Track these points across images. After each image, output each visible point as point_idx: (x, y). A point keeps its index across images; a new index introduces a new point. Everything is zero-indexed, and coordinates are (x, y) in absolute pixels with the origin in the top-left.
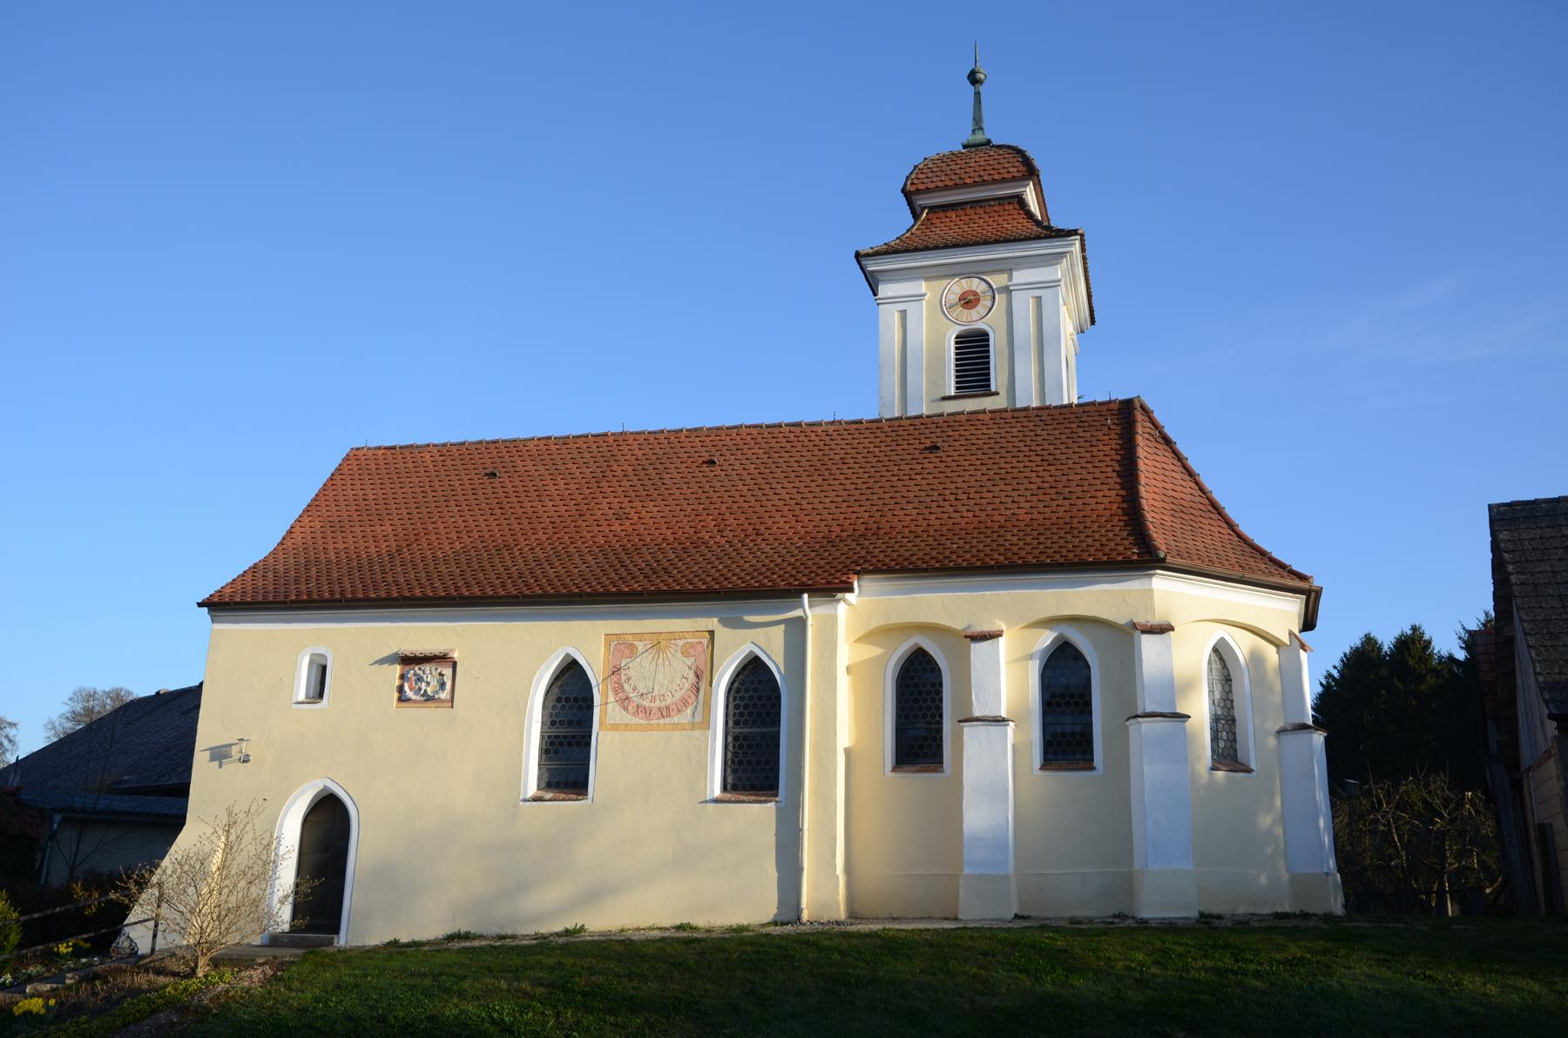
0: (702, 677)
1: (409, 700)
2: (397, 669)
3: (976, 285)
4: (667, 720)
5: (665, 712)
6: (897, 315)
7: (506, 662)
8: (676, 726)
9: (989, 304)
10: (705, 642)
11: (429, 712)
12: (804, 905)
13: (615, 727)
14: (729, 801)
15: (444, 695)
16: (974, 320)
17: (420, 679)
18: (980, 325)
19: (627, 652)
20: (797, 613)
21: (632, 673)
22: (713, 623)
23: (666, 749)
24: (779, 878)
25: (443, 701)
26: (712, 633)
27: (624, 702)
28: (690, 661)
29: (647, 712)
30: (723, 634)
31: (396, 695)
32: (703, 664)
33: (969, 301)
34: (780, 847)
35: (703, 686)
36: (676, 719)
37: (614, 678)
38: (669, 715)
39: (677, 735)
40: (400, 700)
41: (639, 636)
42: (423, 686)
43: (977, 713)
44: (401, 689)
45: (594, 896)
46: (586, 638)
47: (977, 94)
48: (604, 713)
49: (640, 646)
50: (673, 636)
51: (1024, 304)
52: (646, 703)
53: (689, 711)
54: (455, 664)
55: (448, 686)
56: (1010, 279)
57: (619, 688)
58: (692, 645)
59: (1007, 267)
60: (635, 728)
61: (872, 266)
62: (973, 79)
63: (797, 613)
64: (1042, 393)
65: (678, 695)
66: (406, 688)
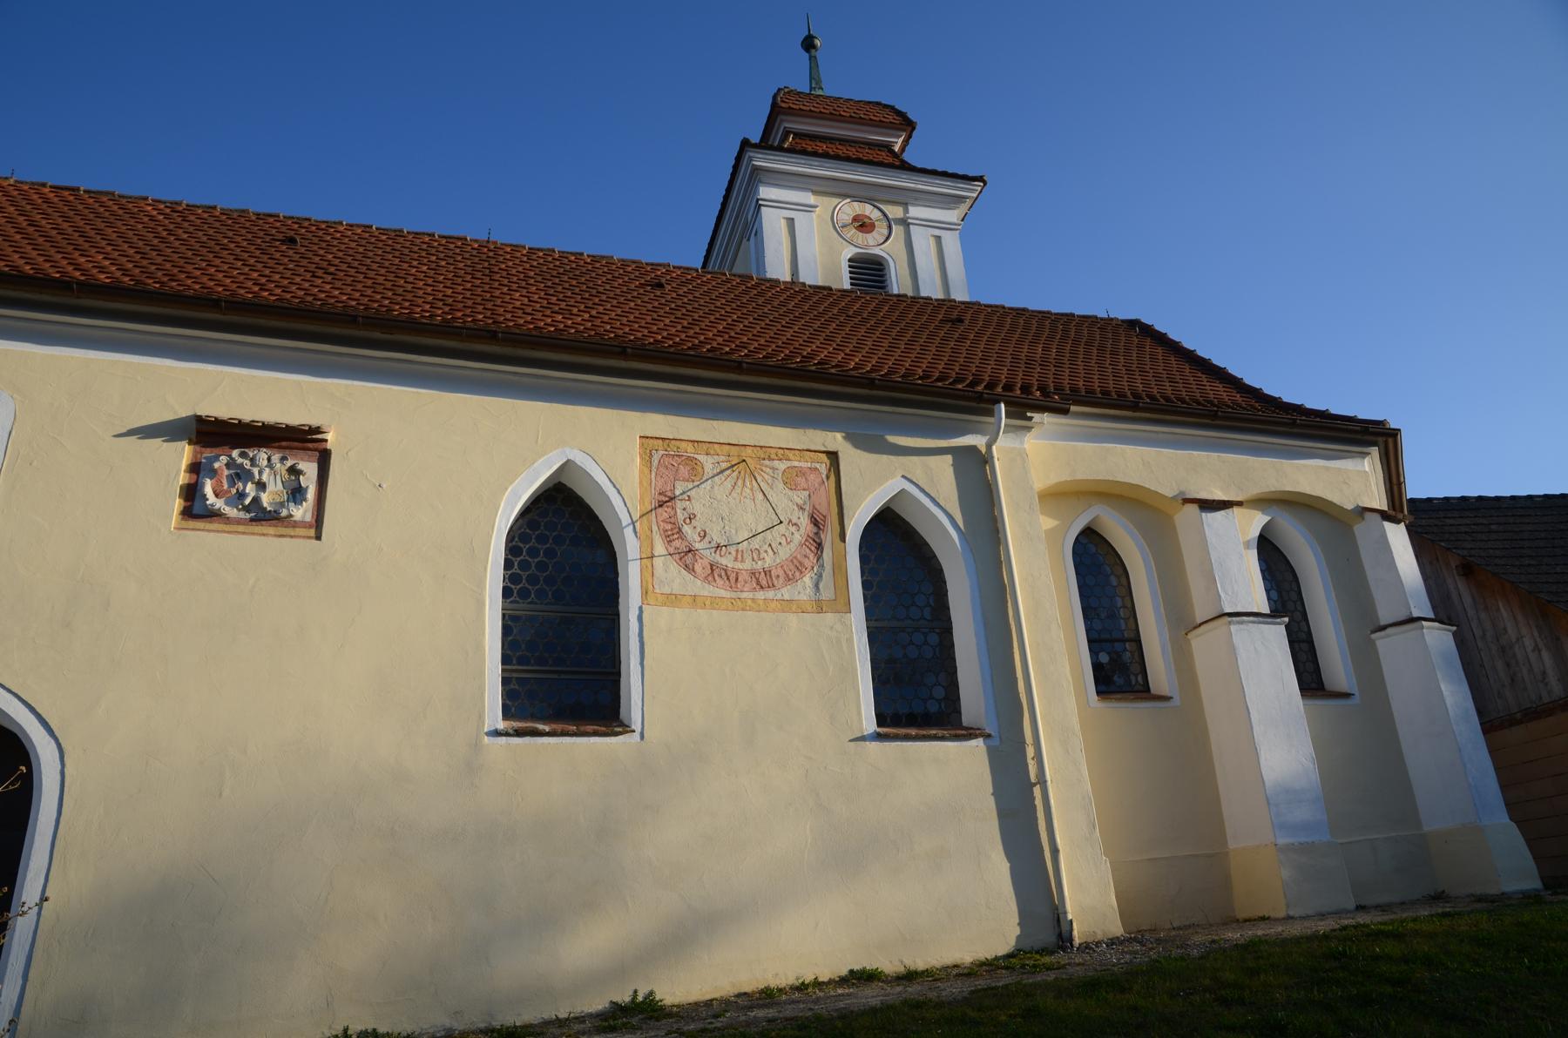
0: (821, 527)
1: (212, 515)
2: (184, 453)
3: (868, 210)
4: (770, 594)
5: (763, 579)
6: (783, 223)
7: (438, 470)
9: (886, 232)
10: (823, 469)
11: (261, 545)
12: (1075, 933)
13: (672, 600)
14: (896, 738)
15: (302, 512)
16: (872, 244)
17: (240, 475)
18: (877, 251)
19: (684, 471)
20: (978, 441)
21: (696, 507)
22: (836, 440)
23: (740, 638)
24: (1012, 869)
25: (296, 525)
26: (833, 456)
27: (685, 557)
28: (800, 497)
29: (714, 571)
30: (852, 459)
31: (178, 504)
33: (864, 225)
34: (1003, 814)
35: (828, 538)
36: (786, 593)
37: (664, 513)
38: (771, 586)
39: (793, 620)
40: (188, 513)
41: (708, 446)
42: (250, 488)
43: (1383, 622)
44: (191, 493)
45: (682, 937)
46: (606, 445)
47: (812, 59)
49: (708, 463)
50: (767, 453)
51: (923, 241)
52: (726, 561)
53: (808, 580)
54: (324, 459)
55: (311, 494)
56: (906, 211)
57: (673, 533)
58: (801, 472)
59: (904, 198)
60: (714, 603)
62: (808, 44)
63: (978, 441)
65: (785, 553)
66: (208, 489)
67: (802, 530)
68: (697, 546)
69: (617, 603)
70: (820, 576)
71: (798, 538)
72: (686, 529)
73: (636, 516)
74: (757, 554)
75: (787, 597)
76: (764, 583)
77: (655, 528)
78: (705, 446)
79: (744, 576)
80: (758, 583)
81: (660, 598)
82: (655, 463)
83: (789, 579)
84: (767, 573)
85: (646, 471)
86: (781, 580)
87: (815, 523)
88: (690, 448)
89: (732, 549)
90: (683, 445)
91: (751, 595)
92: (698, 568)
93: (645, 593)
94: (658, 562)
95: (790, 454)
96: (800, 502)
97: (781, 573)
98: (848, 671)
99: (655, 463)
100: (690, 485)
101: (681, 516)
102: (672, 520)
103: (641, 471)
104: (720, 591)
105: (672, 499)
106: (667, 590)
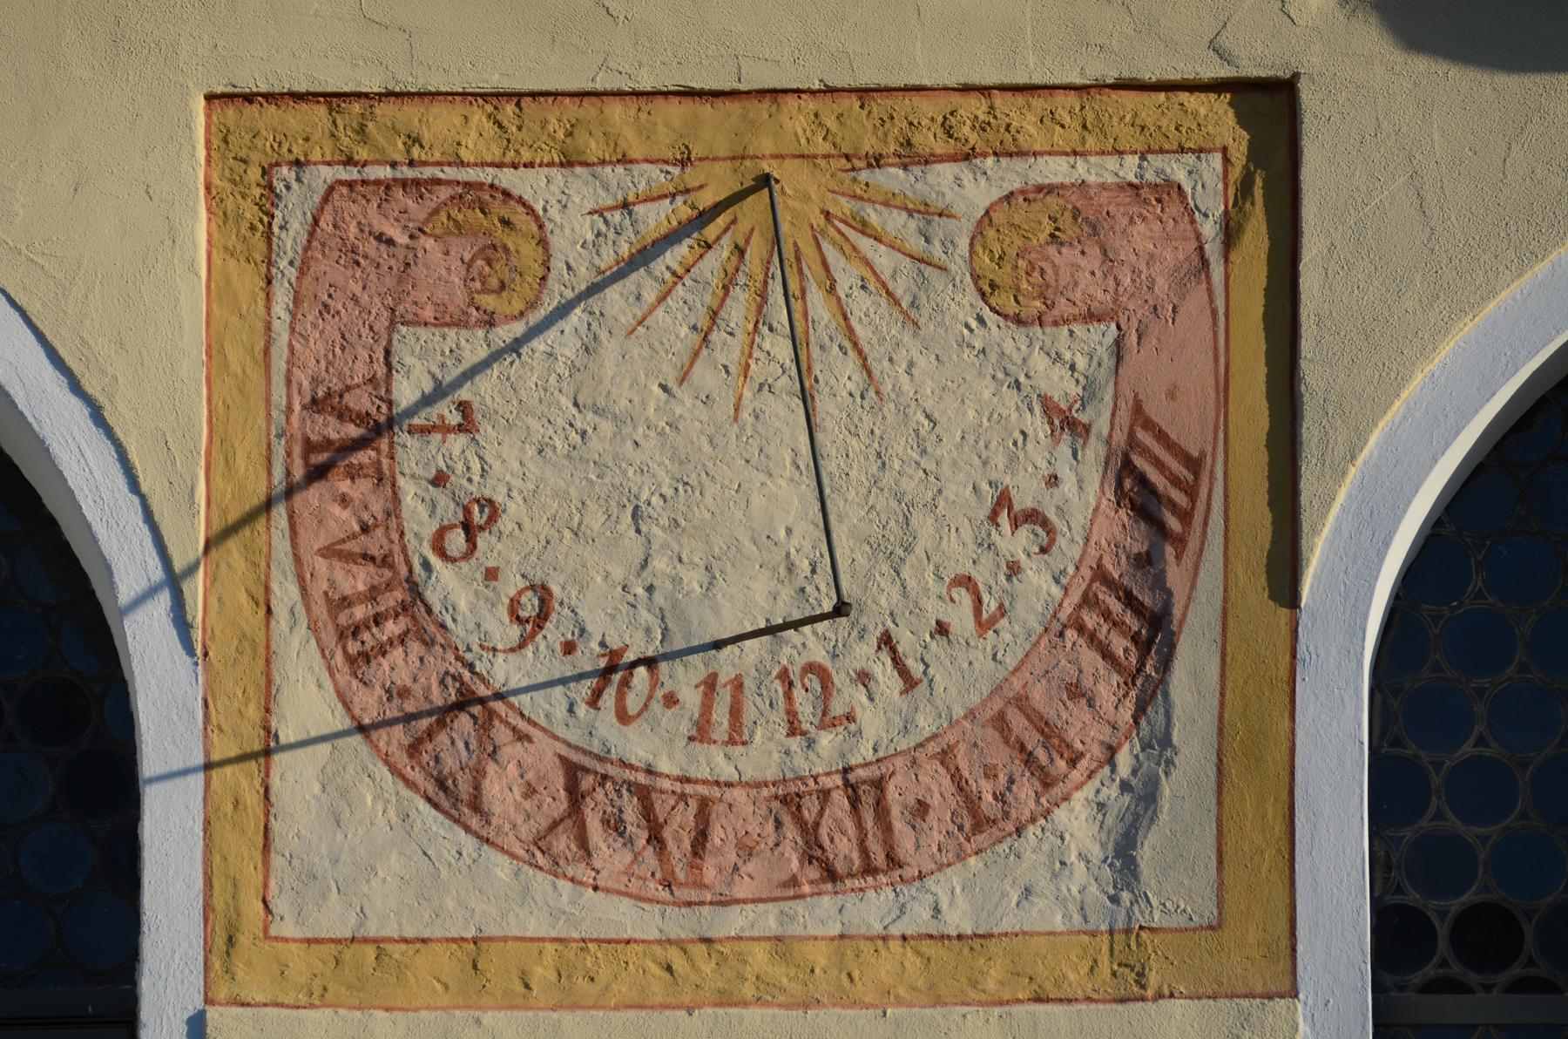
0: (1179, 517)
4: (871, 908)
8: (960, 962)
10: (1206, 184)
13: (362, 965)
19: (442, 267)
21: (504, 463)
27: (441, 732)
28: (1063, 361)
32: (1197, 376)
35: (1203, 590)
36: (956, 897)
37: (330, 511)
38: (879, 864)
48: (247, 832)
49: (571, 212)
52: (652, 744)
53: (1079, 821)
57: (380, 610)
58: (1080, 217)
61: (1143, 436)
64: (151, 781)
65: (963, 679)
67: (1068, 548)
68: (504, 672)
69: (43, 506)
70: (1145, 796)
71: (1040, 590)
72: (450, 587)
73: (187, 544)
74: (815, 696)
75: (958, 919)
76: (843, 849)
77: (285, 593)
78: (555, 118)
79: (742, 816)
80: (813, 850)
81: (299, 962)
82: (291, 239)
83: (978, 821)
84: (864, 792)
85: (247, 281)
86: (938, 826)
87: (1138, 495)
88: (474, 134)
89: (684, 679)
90: (440, 124)
91: (768, 919)
92: (500, 791)
93: (223, 940)
94: (296, 776)
95: (1024, 118)
96: (1063, 387)
97: (936, 786)
98: (1365, 1016)
99: (291, 239)
100: (474, 346)
101: (420, 514)
102: (374, 546)
103: (218, 289)
104: (611, 907)
105: (379, 429)
106: (335, 920)
